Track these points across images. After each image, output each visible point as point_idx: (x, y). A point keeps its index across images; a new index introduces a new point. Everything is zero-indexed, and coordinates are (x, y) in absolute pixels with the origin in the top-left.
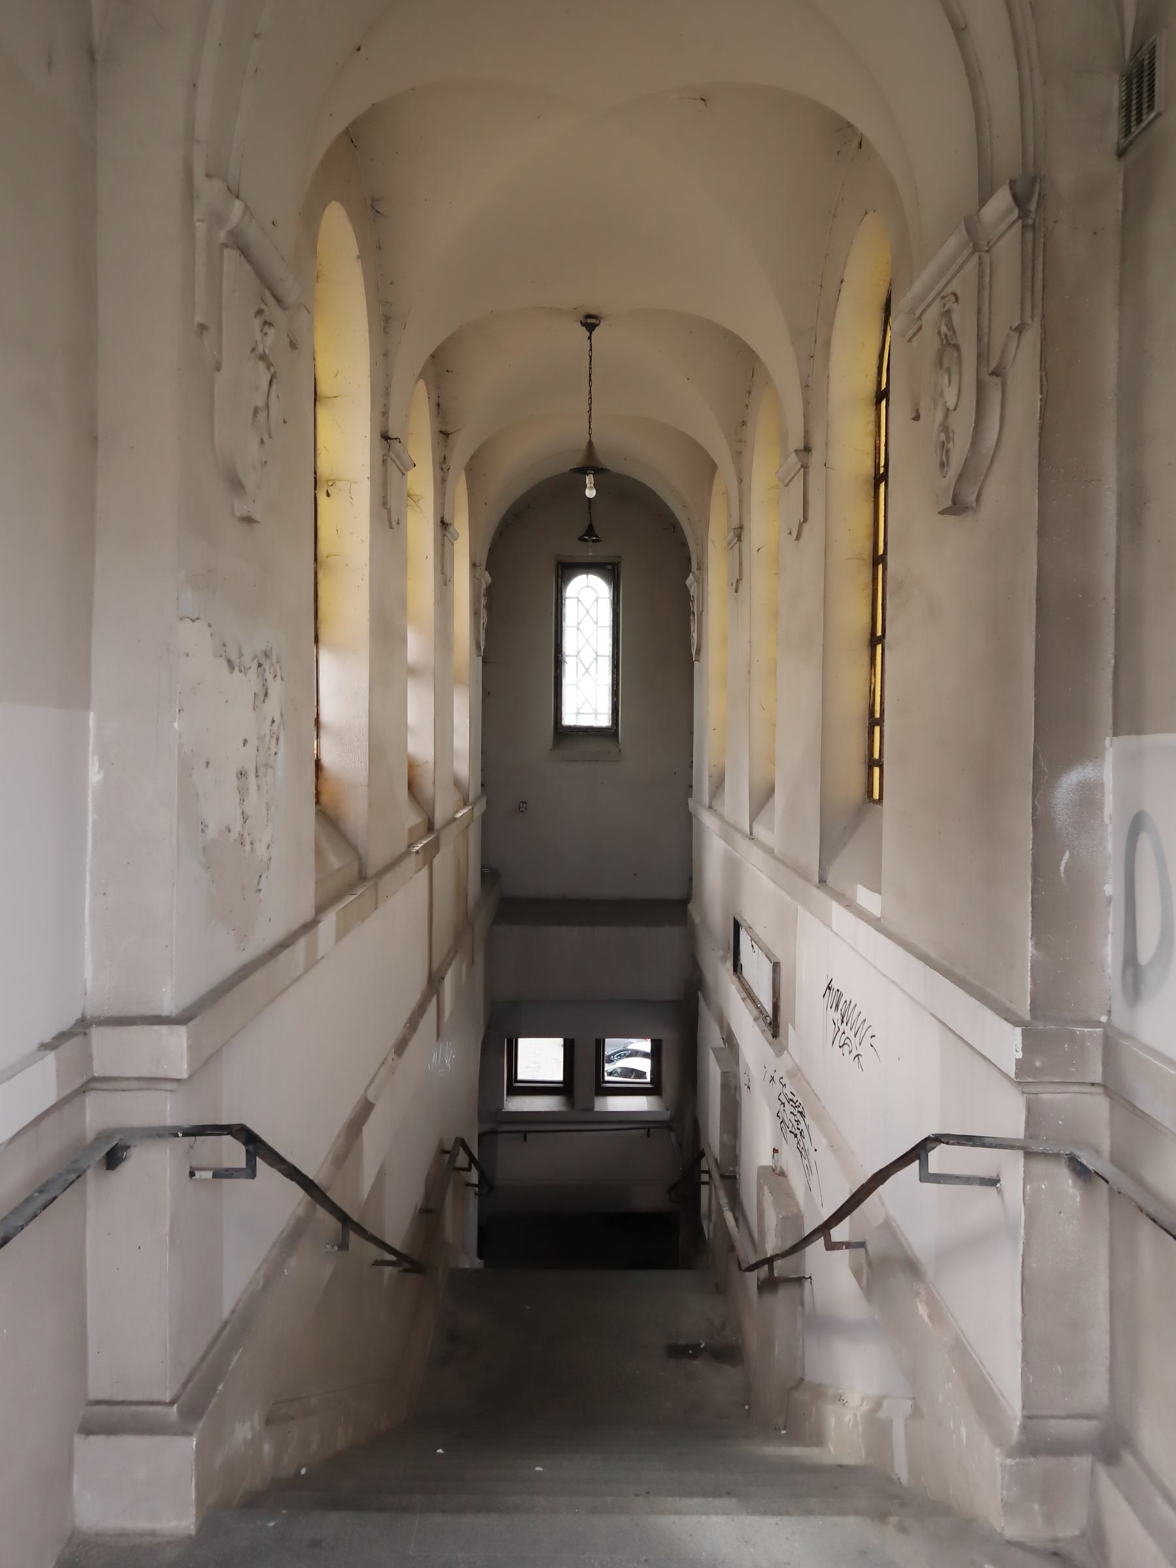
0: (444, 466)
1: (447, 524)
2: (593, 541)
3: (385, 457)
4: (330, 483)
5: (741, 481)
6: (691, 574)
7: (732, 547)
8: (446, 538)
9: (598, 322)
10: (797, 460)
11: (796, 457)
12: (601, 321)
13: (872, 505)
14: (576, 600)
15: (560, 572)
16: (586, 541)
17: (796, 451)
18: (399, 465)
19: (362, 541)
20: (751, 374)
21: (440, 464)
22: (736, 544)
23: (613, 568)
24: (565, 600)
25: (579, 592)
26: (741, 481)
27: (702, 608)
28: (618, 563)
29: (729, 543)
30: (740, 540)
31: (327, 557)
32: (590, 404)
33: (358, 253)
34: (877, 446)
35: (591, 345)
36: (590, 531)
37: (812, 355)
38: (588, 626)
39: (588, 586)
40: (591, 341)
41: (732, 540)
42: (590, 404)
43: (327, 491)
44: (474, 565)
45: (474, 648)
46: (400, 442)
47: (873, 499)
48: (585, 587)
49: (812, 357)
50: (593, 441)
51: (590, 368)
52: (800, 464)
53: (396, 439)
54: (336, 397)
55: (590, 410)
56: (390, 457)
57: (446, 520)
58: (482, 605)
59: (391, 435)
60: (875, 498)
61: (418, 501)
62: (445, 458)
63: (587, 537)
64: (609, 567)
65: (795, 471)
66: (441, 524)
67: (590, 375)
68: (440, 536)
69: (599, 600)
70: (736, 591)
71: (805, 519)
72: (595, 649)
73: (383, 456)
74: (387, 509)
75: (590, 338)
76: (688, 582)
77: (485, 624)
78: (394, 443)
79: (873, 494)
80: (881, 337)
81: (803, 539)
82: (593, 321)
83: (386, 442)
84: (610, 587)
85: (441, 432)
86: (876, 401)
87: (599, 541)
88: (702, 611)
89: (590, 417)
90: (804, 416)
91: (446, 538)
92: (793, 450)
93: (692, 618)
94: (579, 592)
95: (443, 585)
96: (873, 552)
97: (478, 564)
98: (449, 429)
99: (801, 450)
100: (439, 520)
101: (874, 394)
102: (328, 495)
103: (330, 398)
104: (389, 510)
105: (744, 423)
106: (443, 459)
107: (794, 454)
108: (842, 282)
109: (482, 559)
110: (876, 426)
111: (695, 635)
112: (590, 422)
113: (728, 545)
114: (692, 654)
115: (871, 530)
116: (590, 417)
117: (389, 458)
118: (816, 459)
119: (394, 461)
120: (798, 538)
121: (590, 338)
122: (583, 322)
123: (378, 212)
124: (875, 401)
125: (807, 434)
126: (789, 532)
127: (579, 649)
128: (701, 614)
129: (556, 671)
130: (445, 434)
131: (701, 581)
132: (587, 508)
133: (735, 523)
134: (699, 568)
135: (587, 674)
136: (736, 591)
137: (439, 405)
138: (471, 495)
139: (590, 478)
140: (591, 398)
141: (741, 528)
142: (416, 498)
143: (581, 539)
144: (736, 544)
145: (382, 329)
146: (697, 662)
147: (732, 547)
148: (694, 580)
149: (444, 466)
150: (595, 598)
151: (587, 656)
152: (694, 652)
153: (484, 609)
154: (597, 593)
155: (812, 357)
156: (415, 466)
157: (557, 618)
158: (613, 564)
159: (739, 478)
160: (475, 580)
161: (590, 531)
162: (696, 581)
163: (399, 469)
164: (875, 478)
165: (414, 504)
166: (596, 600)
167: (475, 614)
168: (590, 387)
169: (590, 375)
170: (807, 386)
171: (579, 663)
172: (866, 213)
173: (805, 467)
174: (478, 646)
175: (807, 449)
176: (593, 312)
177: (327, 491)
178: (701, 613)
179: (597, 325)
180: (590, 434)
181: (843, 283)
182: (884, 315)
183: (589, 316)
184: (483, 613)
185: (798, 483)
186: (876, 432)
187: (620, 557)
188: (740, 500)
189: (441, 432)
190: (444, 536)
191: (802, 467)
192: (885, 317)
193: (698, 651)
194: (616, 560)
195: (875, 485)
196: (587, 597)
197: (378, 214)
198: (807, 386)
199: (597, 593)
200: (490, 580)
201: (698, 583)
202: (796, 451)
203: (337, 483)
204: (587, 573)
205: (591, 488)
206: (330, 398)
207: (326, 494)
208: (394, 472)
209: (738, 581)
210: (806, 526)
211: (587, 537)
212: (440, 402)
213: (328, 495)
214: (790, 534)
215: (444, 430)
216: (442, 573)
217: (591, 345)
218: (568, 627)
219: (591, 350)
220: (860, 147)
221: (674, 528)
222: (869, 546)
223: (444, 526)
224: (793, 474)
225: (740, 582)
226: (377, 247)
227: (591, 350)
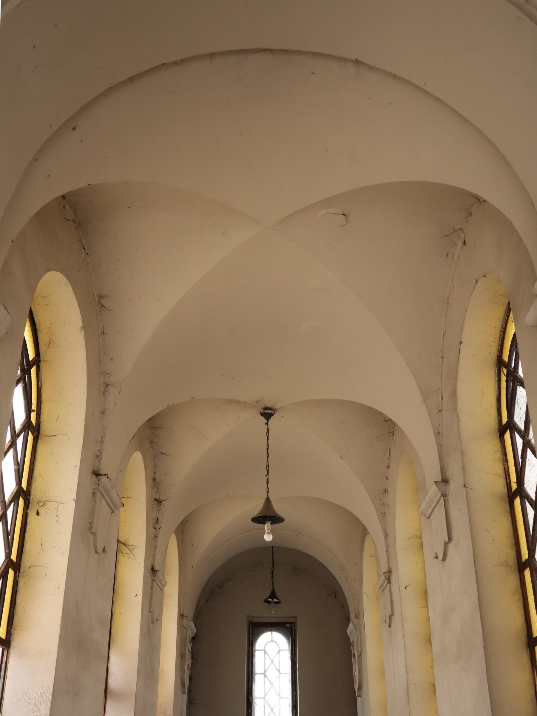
0: (157, 526)
1: (156, 571)
2: (276, 603)
3: (95, 491)
4: (41, 504)
5: (386, 535)
6: (351, 623)
7: (383, 590)
8: (154, 582)
9: (273, 412)
10: (438, 490)
11: (436, 488)
12: (276, 413)
13: (510, 519)
14: (263, 652)
15: (251, 630)
16: (270, 602)
17: (436, 482)
18: (109, 501)
19: (63, 554)
20: (389, 453)
21: (154, 524)
22: (386, 586)
23: (291, 626)
24: (255, 652)
25: (265, 646)
26: (387, 535)
27: (361, 650)
28: (295, 622)
29: (381, 587)
30: (389, 582)
31: (29, 568)
32: (268, 470)
33: (82, 325)
34: (506, 470)
35: (268, 428)
36: (273, 595)
37: (440, 409)
38: (272, 673)
39: (272, 641)
40: (268, 426)
41: (383, 584)
42: (268, 470)
43: (38, 511)
44: (181, 616)
45: (179, 687)
46: (108, 477)
47: (509, 514)
48: (270, 641)
49: (440, 411)
50: (270, 497)
51: (268, 445)
52: (440, 493)
53: (105, 475)
54: (55, 436)
55: (268, 474)
56: (99, 490)
57: (156, 568)
58: (187, 650)
59: (102, 472)
60: (511, 512)
61: (133, 549)
62: (158, 520)
63: (270, 600)
64: (288, 626)
65: (436, 501)
66: (151, 571)
67: (267, 449)
68: (149, 581)
69: (281, 652)
70: (390, 626)
71: (450, 539)
72: (278, 693)
73: (94, 489)
74: (92, 533)
75: (267, 424)
76: (349, 631)
77: (190, 666)
78: (103, 479)
79: (508, 509)
80: (497, 386)
81: (448, 559)
82: (269, 411)
83: (96, 477)
84: (289, 642)
85: (155, 500)
86: (500, 435)
87: (280, 603)
88: (361, 652)
89: (268, 479)
90: (439, 457)
91: (154, 582)
92: (434, 481)
93: (353, 659)
94: (265, 646)
95: (150, 623)
96: (517, 559)
97: (185, 615)
98: (162, 497)
99: (440, 481)
100: (149, 567)
101: (497, 430)
102: (38, 514)
103: (50, 436)
104: (94, 534)
105: (386, 491)
106: (156, 520)
107: (434, 485)
108: (461, 343)
109: (190, 612)
110: (503, 454)
111: (356, 674)
112: (267, 484)
113: (380, 589)
114: (355, 691)
115: (512, 540)
116: (268, 479)
117: (98, 492)
118: (454, 487)
119: (103, 496)
120: (444, 559)
121: (267, 424)
122: (262, 412)
123: (103, 306)
124: (499, 435)
125: (443, 469)
126: (435, 556)
127: (266, 691)
128: (360, 655)
129: (247, 711)
130: (159, 501)
131: (359, 628)
132: (271, 577)
133: (384, 569)
134: (357, 617)
135: (272, 713)
136: (390, 626)
137: (155, 479)
138: (182, 561)
139: (268, 525)
140: (268, 466)
141: (390, 572)
142: (130, 547)
143: (266, 601)
144: (386, 586)
145: (102, 393)
146: (359, 698)
147: (383, 590)
148: (353, 628)
149: (157, 526)
150: (278, 650)
151: (272, 698)
152: (356, 689)
153: (189, 654)
154: (279, 646)
155: (440, 411)
156: (123, 506)
157: (248, 666)
158: (291, 623)
159: (385, 533)
160: (181, 628)
161: (273, 595)
162: (355, 628)
163: (109, 505)
164: (508, 496)
165: (130, 552)
166: (279, 652)
167: (181, 656)
168: (268, 458)
169: (267, 449)
170: (438, 433)
171: (266, 705)
172: (477, 282)
173: (444, 495)
174: (183, 685)
175: (445, 481)
176: (269, 405)
177: (38, 511)
178: (360, 655)
179: (273, 415)
180: (268, 492)
181: (462, 344)
182: (497, 369)
183: (266, 408)
184: (188, 656)
185: (440, 512)
186: (503, 460)
187: (295, 617)
188: (387, 551)
189: (155, 500)
190: (153, 580)
191: (442, 495)
192: (498, 370)
193: (360, 688)
194: (292, 620)
195: (509, 501)
196: (272, 649)
197: (103, 308)
198: (438, 433)
199: (279, 646)
200: (195, 630)
201: (356, 630)
202: (436, 482)
203: (47, 504)
204: (271, 630)
205: (268, 533)
206: (50, 436)
207: (36, 513)
208: (103, 508)
209: (391, 616)
210: (451, 546)
211: (270, 600)
212: (156, 477)
213: (38, 514)
214: (436, 557)
215: (158, 498)
216: (150, 612)
217: (268, 428)
218: (257, 674)
219: (268, 432)
220: (465, 244)
221: (335, 594)
222: (512, 553)
223: (153, 572)
224: (434, 505)
225: (392, 617)
226: (101, 332)
227: (268, 432)
